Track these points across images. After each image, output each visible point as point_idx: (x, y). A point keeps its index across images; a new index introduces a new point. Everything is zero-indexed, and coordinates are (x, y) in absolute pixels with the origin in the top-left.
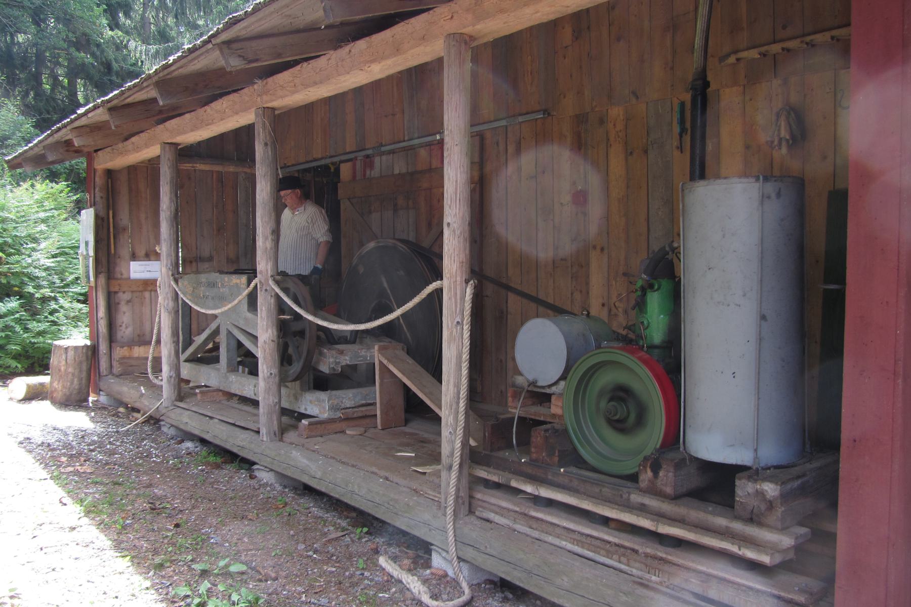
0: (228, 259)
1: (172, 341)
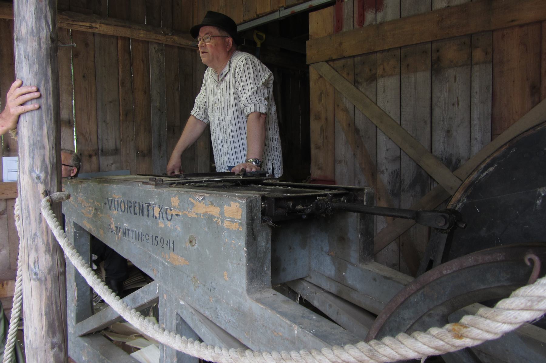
0: (137, 150)
1: (49, 345)
